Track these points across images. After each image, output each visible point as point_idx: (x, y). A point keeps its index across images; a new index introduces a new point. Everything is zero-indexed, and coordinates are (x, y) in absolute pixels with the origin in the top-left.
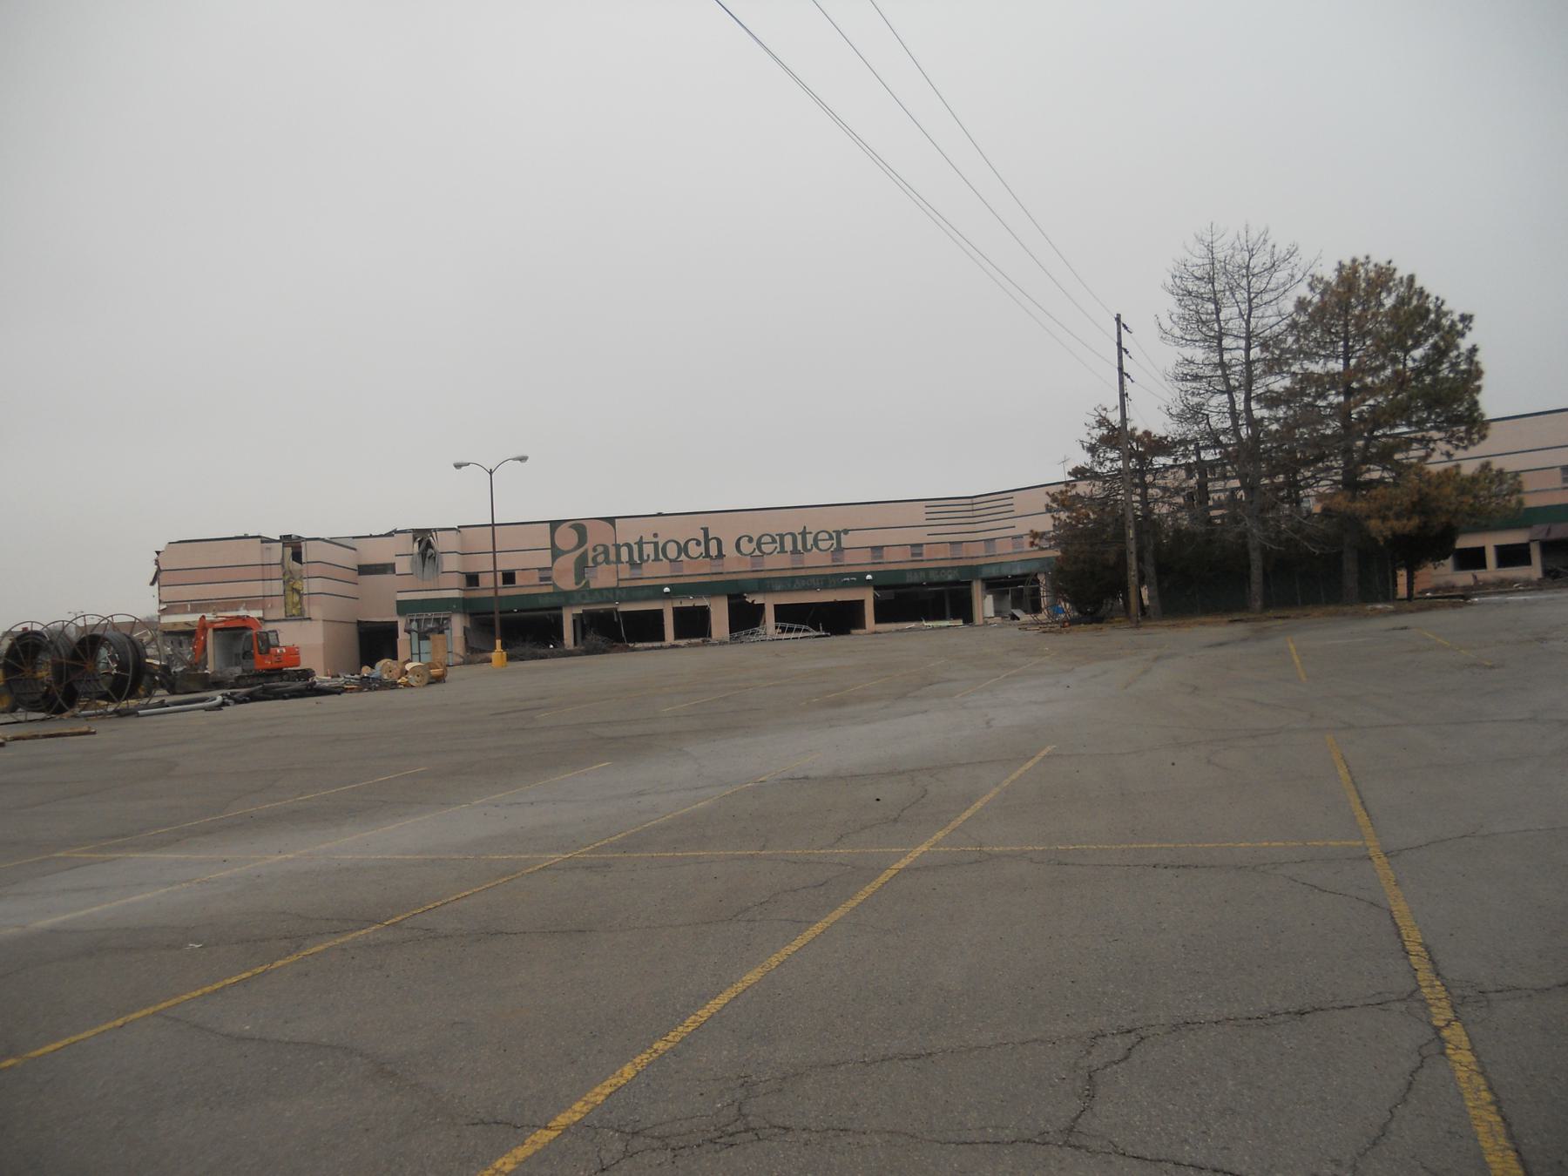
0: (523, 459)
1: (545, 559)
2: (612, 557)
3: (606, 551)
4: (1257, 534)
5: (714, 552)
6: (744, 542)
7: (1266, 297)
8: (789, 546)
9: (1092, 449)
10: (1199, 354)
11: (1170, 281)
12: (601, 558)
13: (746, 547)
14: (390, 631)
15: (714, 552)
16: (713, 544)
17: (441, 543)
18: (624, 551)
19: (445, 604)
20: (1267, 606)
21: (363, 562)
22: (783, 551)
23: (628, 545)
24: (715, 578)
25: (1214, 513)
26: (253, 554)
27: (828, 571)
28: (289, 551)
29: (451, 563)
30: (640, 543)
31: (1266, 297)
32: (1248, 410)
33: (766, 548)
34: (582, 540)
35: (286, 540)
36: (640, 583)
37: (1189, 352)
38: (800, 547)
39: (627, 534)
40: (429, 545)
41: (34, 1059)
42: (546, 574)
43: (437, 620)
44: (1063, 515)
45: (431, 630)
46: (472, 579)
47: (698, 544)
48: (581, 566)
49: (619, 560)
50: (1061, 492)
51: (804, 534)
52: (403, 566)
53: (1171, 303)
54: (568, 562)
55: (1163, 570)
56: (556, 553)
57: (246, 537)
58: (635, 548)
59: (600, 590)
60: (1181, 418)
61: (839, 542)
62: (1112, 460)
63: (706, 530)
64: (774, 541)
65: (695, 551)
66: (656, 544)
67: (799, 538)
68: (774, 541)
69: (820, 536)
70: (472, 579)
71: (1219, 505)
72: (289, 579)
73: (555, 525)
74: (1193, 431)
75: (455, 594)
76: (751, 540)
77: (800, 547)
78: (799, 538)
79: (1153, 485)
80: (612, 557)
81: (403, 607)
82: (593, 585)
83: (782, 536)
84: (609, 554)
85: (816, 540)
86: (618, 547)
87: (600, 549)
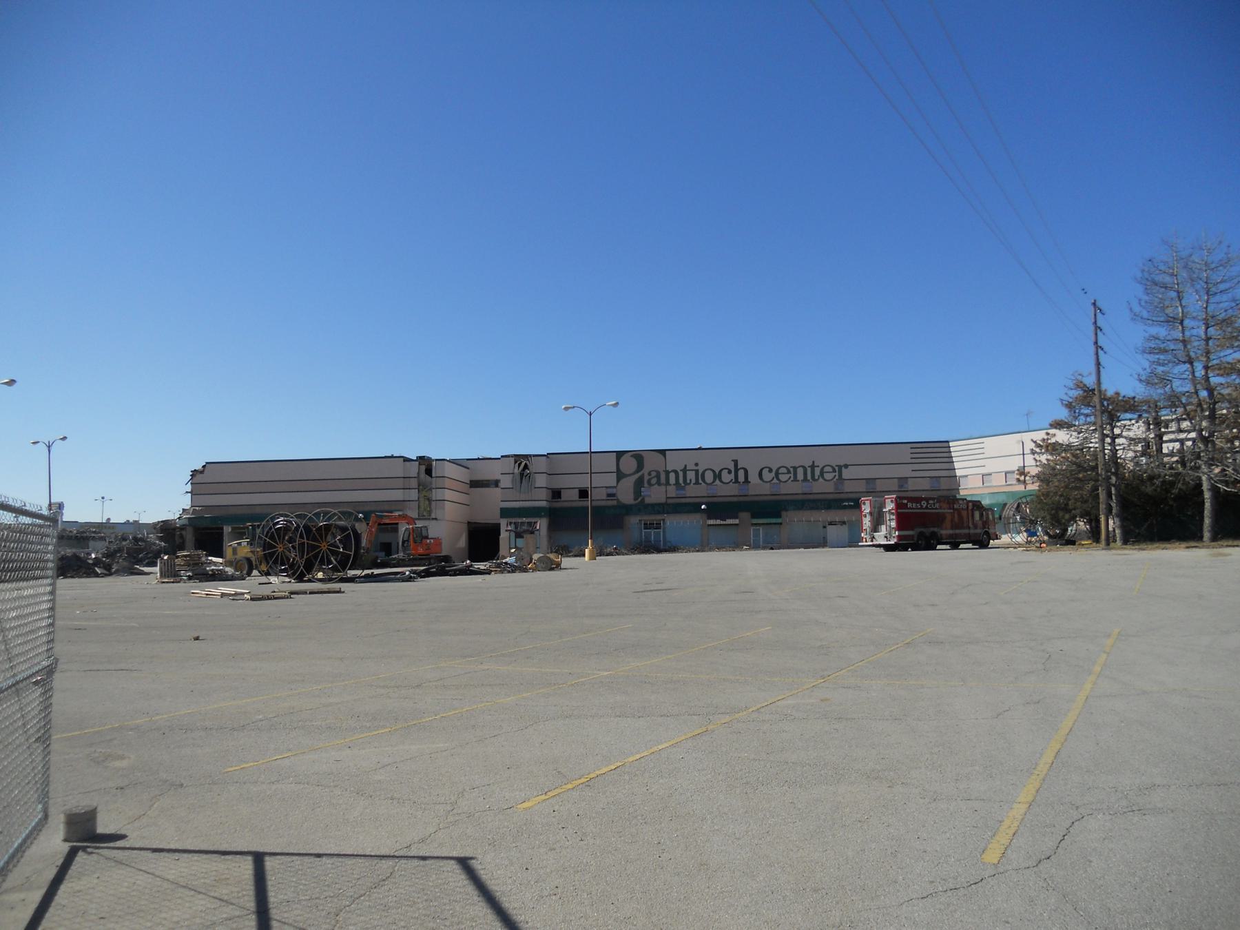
0: (64, 438)
1: (611, 480)
2: (663, 480)
3: (658, 476)
4: (1208, 476)
5: (741, 478)
6: (765, 472)
7: (1222, 287)
8: (800, 476)
9: (1069, 406)
10: (1162, 332)
11: (1139, 275)
12: (654, 481)
13: (767, 476)
14: (494, 530)
15: (741, 478)
16: (741, 473)
17: (535, 466)
18: (672, 476)
19: (535, 512)
20: (1214, 539)
21: (474, 478)
22: (795, 480)
23: (676, 472)
24: (741, 499)
25: (1166, 459)
26: (398, 470)
27: (831, 497)
28: (423, 468)
29: (541, 481)
30: (685, 470)
31: (1222, 287)
32: (1207, 379)
33: (783, 478)
34: (640, 466)
35: (421, 459)
36: (683, 501)
37: (1154, 330)
38: (809, 477)
39: (673, 463)
40: (526, 467)
41: (525, 809)
42: (610, 491)
43: (529, 524)
44: (1044, 458)
45: (525, 531)
46: (556, 494)
47: (730, 472)
48: (639, 483)
49: (668, 483)
50: (1043, 440)
51: (813, 467)
52: (506, 482)
53: (1139, 290)
54: (628, 483)
55: (1125, 504)
56: (620, 475)
57: (392, 457)
58: (681, 474)
59: (653, 505)
60: (1148, 383)
61: (840, 475)
62: (1087, 415)
63: (736, 462)
64: (789, 472)
65: (726, 477)
66: (697, 471)
67: (809, 470)
68: (789, 472)
69: (827, 469)
70: (556, 494)
71: (1171, 454)
72: (422, 487)
73: (620, 454)
74: (1156, 393)
75: (544, 504)
76: (771, 470)
77: (809, 477)
78: (809, 470)
79: (1120, 436)
80: (663, 480)
81: (505, 513)
82: (647, 501)
83: (795, 468)
84: (660, 478)
85: (822, 473)
86: (667, 473)
87: (654, 474)
